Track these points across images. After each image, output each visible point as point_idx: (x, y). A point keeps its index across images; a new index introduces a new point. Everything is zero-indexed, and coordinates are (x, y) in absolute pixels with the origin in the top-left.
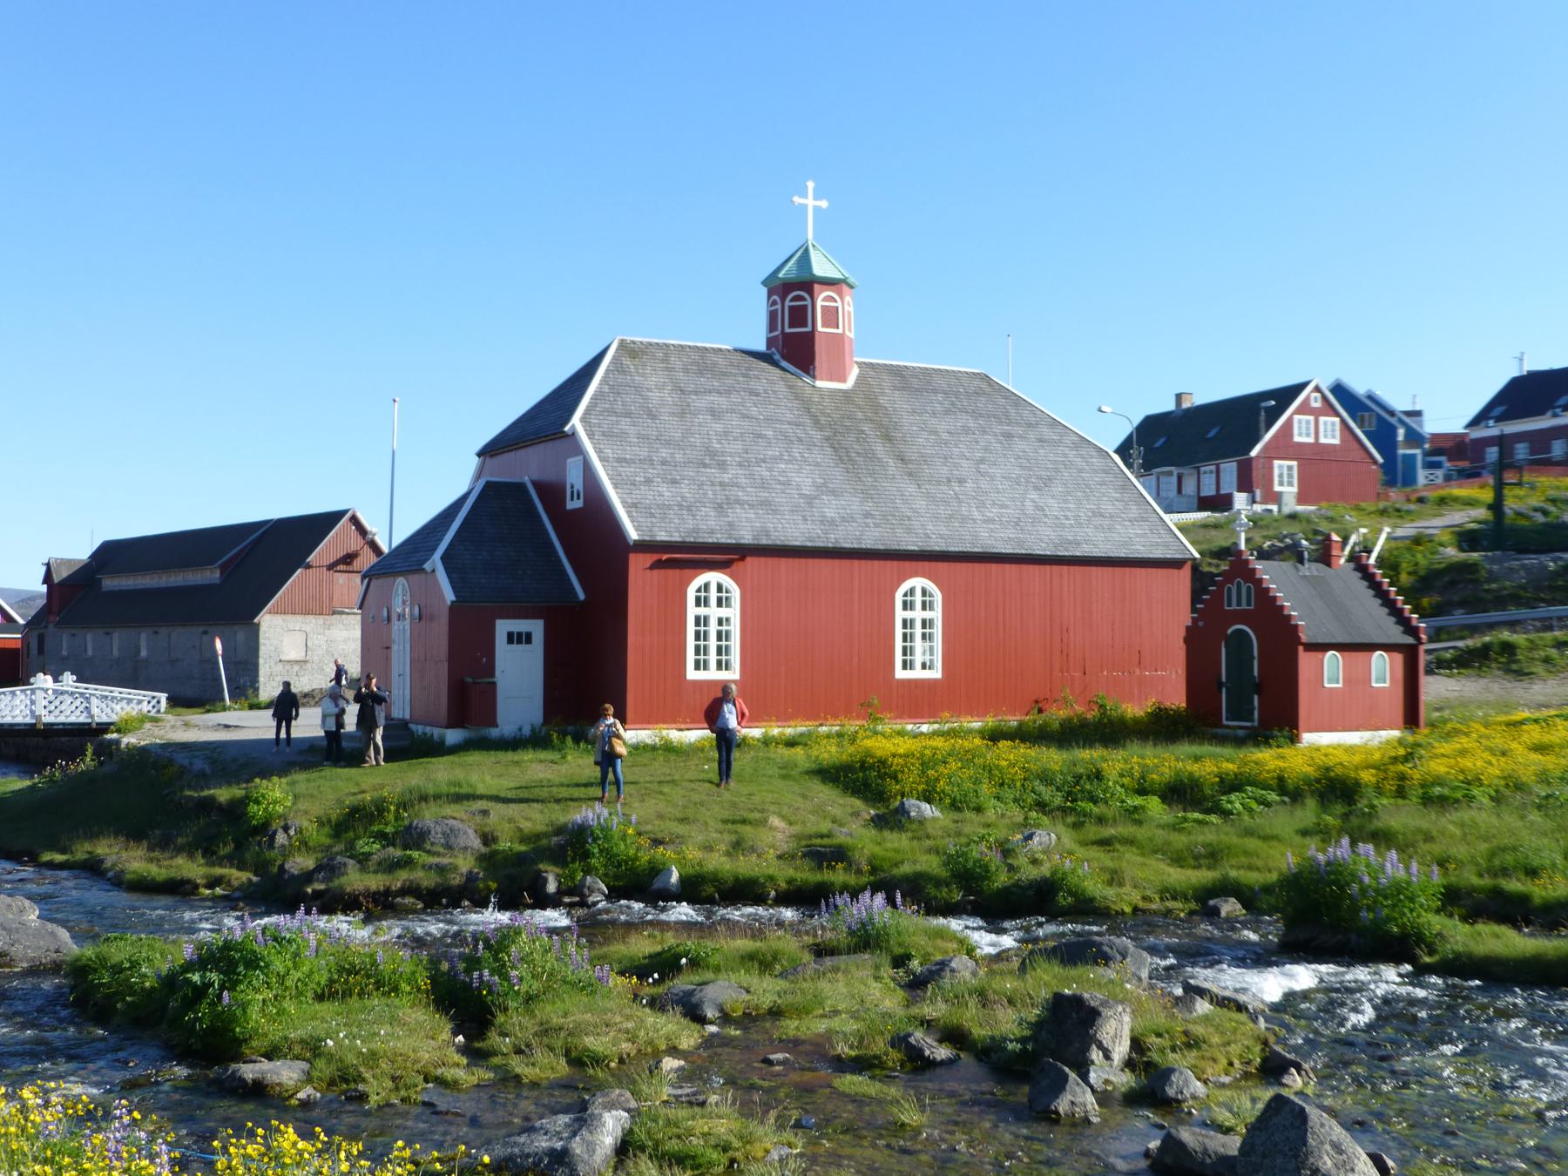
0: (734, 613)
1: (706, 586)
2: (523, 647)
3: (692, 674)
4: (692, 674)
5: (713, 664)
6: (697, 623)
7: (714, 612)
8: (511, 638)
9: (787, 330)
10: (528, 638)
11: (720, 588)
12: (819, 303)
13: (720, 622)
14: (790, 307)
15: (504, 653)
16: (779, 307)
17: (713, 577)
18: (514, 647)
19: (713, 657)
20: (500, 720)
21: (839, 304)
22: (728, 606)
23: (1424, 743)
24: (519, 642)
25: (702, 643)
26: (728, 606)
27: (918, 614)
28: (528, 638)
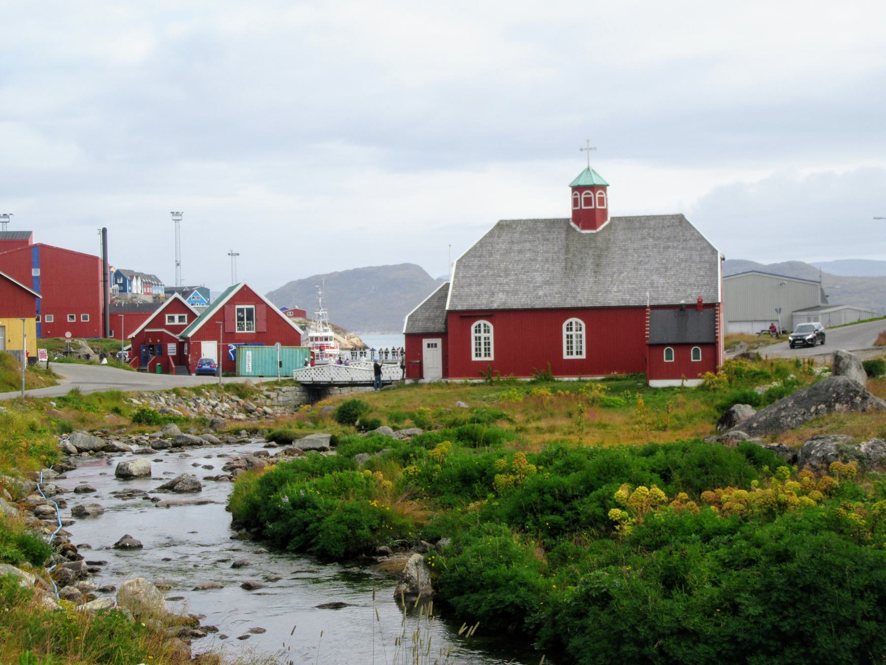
0: (491, 335)
1: (479, 325)
2: (434, 349)
3: (474, 358)
4: (474, 358)
5: (483, 355)
6: (476, 339)
7: (574, 333)
8: (429, 346)
9: (583, 207)
10: (436, 345)
11: (485, 325)
12: (597, 196)
13: (485, 339)
14: (599, 198)
15: (425, 350)
16: (579, 196)
17: (482, 322)
18: (430, 349)
19: (483, 352)
20: (425, 375)
21: (604, 196)
22: (489, 332)
23: (527, 386)
24: (432, 347)
25: (487, 347)
26: (489, 332)
27: (483, 335)
28: (436, 345)
